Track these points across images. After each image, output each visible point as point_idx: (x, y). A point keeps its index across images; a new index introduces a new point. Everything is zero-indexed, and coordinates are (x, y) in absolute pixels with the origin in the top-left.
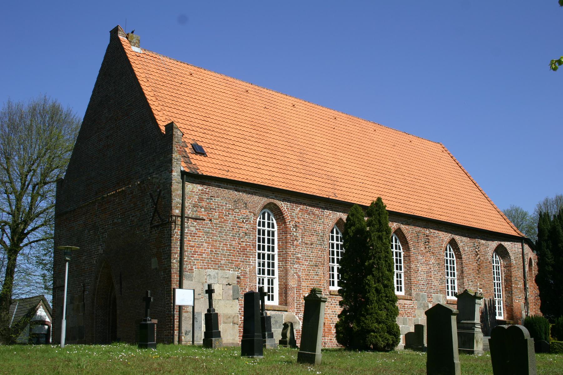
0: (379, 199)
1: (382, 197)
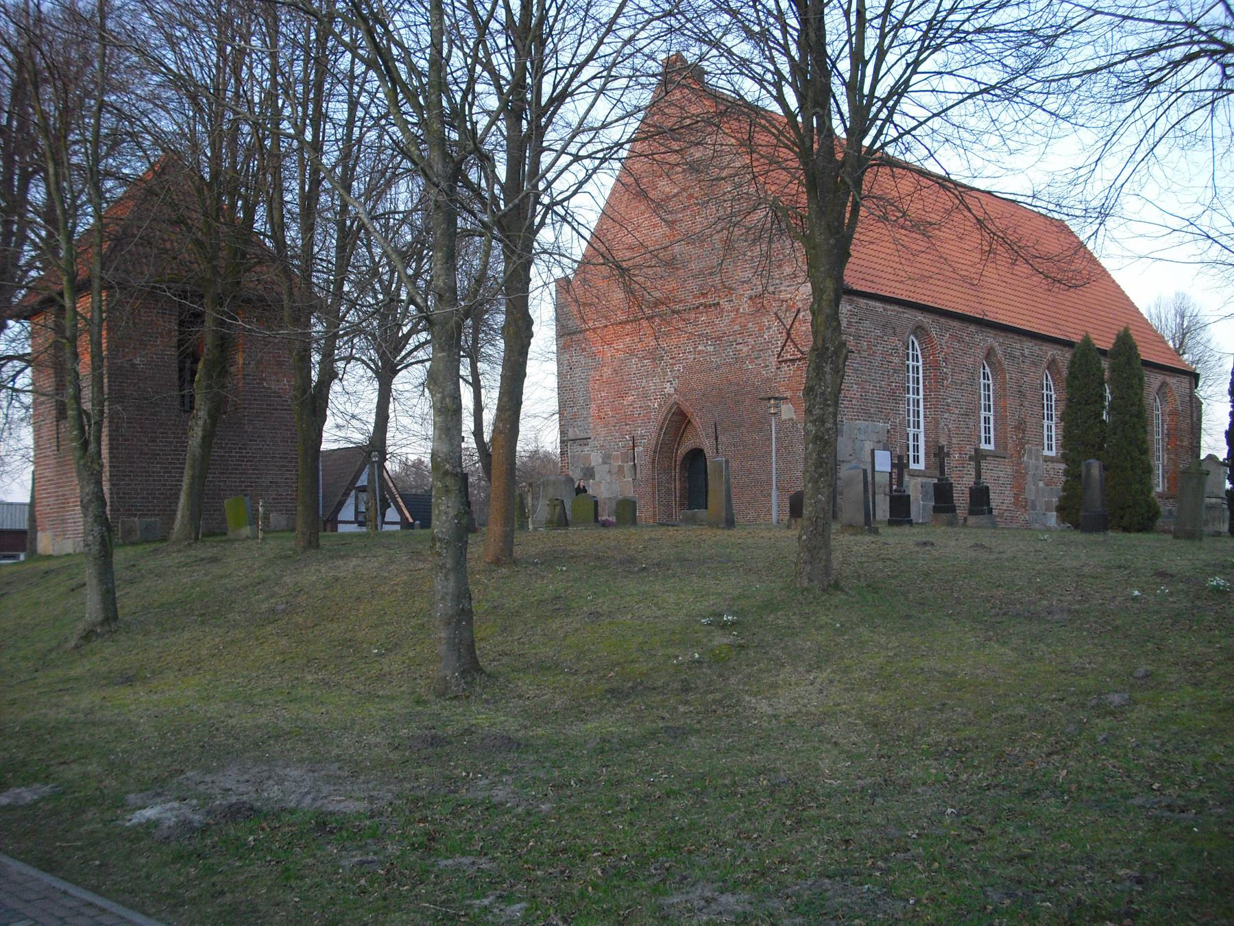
0: (1126, 330)
1: (1131, 327)
